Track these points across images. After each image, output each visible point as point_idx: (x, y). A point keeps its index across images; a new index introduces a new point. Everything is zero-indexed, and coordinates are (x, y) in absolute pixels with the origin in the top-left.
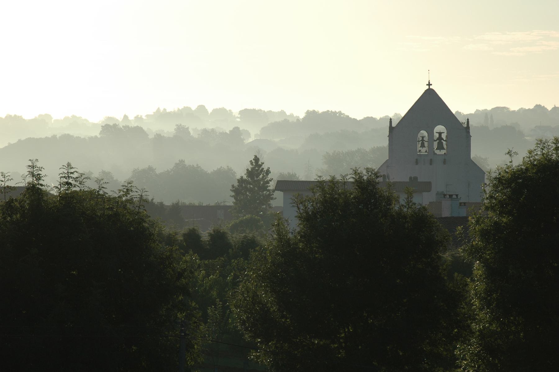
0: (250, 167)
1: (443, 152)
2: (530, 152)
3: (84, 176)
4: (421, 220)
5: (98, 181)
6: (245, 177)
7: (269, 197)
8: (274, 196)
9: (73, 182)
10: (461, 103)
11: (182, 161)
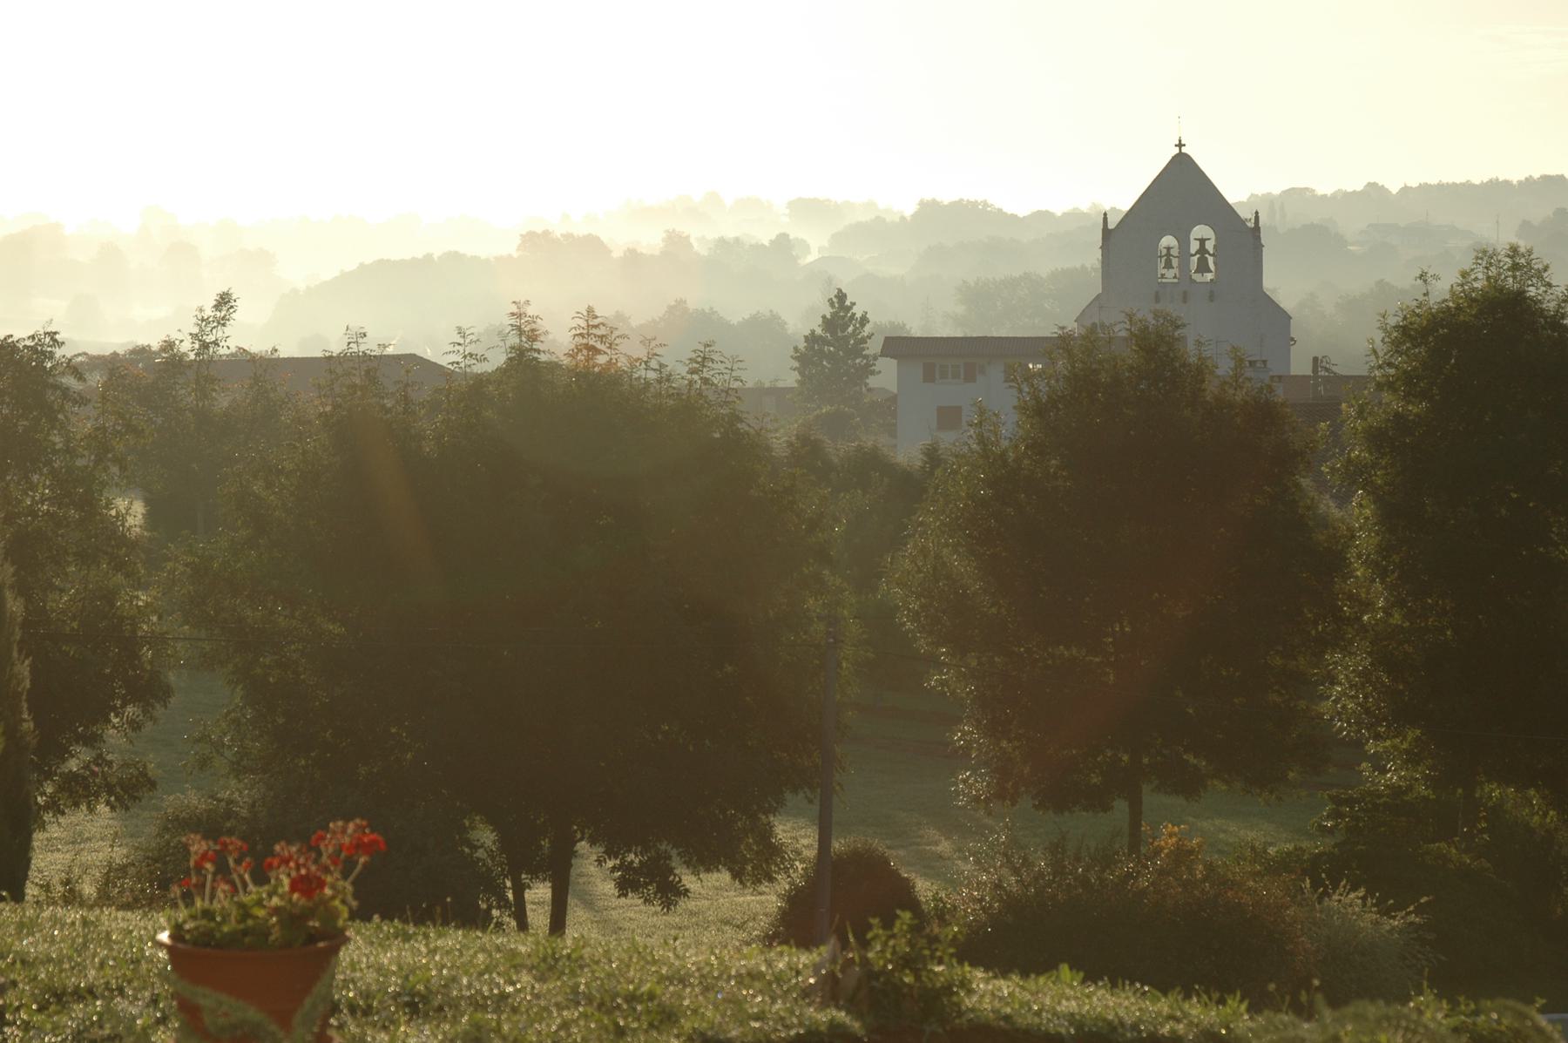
0: (828, 312)
1: (1209, 276)
2: (1464, 275)
3: (616, 333)
4: (1264, 413)
5: (646, 342)
6: (819, 331)
7: (867, 370)
8: (876, 368)
9: (599, 346)
10: (1238, 182)
11: (681, 302)
